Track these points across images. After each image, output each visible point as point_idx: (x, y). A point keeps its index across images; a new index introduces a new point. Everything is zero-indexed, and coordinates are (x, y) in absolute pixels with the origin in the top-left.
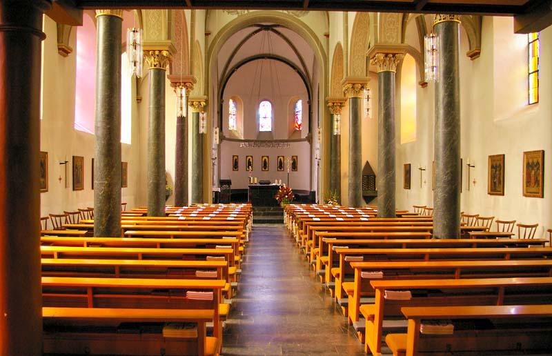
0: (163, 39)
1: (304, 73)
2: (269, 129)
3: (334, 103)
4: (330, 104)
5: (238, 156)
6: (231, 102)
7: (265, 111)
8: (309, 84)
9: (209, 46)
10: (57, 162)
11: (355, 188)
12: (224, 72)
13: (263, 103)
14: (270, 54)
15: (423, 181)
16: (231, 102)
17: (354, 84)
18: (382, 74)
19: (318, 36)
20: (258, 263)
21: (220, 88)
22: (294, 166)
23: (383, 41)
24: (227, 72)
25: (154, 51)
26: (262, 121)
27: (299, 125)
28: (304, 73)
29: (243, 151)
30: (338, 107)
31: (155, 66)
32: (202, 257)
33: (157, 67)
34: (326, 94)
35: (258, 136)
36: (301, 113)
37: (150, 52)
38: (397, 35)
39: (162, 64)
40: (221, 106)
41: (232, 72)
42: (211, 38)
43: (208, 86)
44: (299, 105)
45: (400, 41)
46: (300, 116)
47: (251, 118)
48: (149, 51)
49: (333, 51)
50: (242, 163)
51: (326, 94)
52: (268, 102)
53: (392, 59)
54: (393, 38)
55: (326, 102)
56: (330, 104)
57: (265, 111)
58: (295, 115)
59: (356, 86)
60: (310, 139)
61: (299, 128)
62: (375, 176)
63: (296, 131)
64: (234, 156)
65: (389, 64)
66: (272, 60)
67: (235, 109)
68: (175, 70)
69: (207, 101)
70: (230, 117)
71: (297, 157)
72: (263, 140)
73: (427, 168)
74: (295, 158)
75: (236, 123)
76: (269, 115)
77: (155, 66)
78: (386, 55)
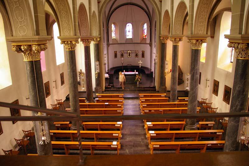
0: (72, 35)
1: (148, 11)
2: (131, 37)
3: (163, 38)
4: (162, 38)
5: (116, 51)
6: (113, 26)
7: (129, 27)
8: (150, 18)
9: (100, 9)
10: (25, 99)
11: (173, 78)
12: (109, 13)
13: (128, 24)
14: (131, 3)
15: (207, 85)
16: (113, 26)
17: (175, 39)
18: (194, 50)
19: (156, 2)
20: (128, 107)
21: (107, 21)
22: (143, 56)
23: (196, 33)
24: (111, 11)
25: (68, 41)
26: (128, 33)
27: (145, 36)
28: (148, 11)
29: (118, 49)
30: (166, 40)
31: (69, 49)
32: (103, 97)
33: (70, 50)
34: (160, 34)
35: (126, 41)
36: (146, 29)
37: (66, 43)
38: (204, 29)
39: (73, 47)
40: (108, 29)
41: (113, 12)
42: (101, 4)
43: (100, 20)
44: (145, 26)
45: (205, 33)
46: (146, 31)
47: (122, 32)
48: (65, 42)
49: (163, 17)
50: (119, 55)
51: (160, 34)
52: (130, 24)
53: (201, 42)
54: (202, 31)
55: (160, 37)
56: (162, 38)
57: (129, 27)
58: (143, 31)
59: (177, 39)
60: (151, 45)
61: (145, 37)
62: (182, 73)
63: (144, 38)
64: (115, 52)
65: (199, 45)
66: (132, 6)
67: (115, 28)
68: (82, 33)
69: (100, 38)
70: (112, 33)
71: (144, 51)
72: (130, 42)
73: (210, 80)
74: (143, 52)
75: (115, 35)
76: (131, 30)
77: (69, 49)
78: (197, 41)
